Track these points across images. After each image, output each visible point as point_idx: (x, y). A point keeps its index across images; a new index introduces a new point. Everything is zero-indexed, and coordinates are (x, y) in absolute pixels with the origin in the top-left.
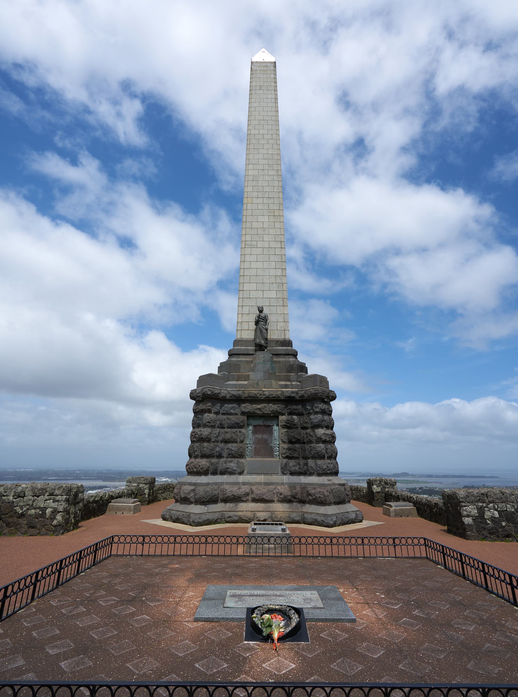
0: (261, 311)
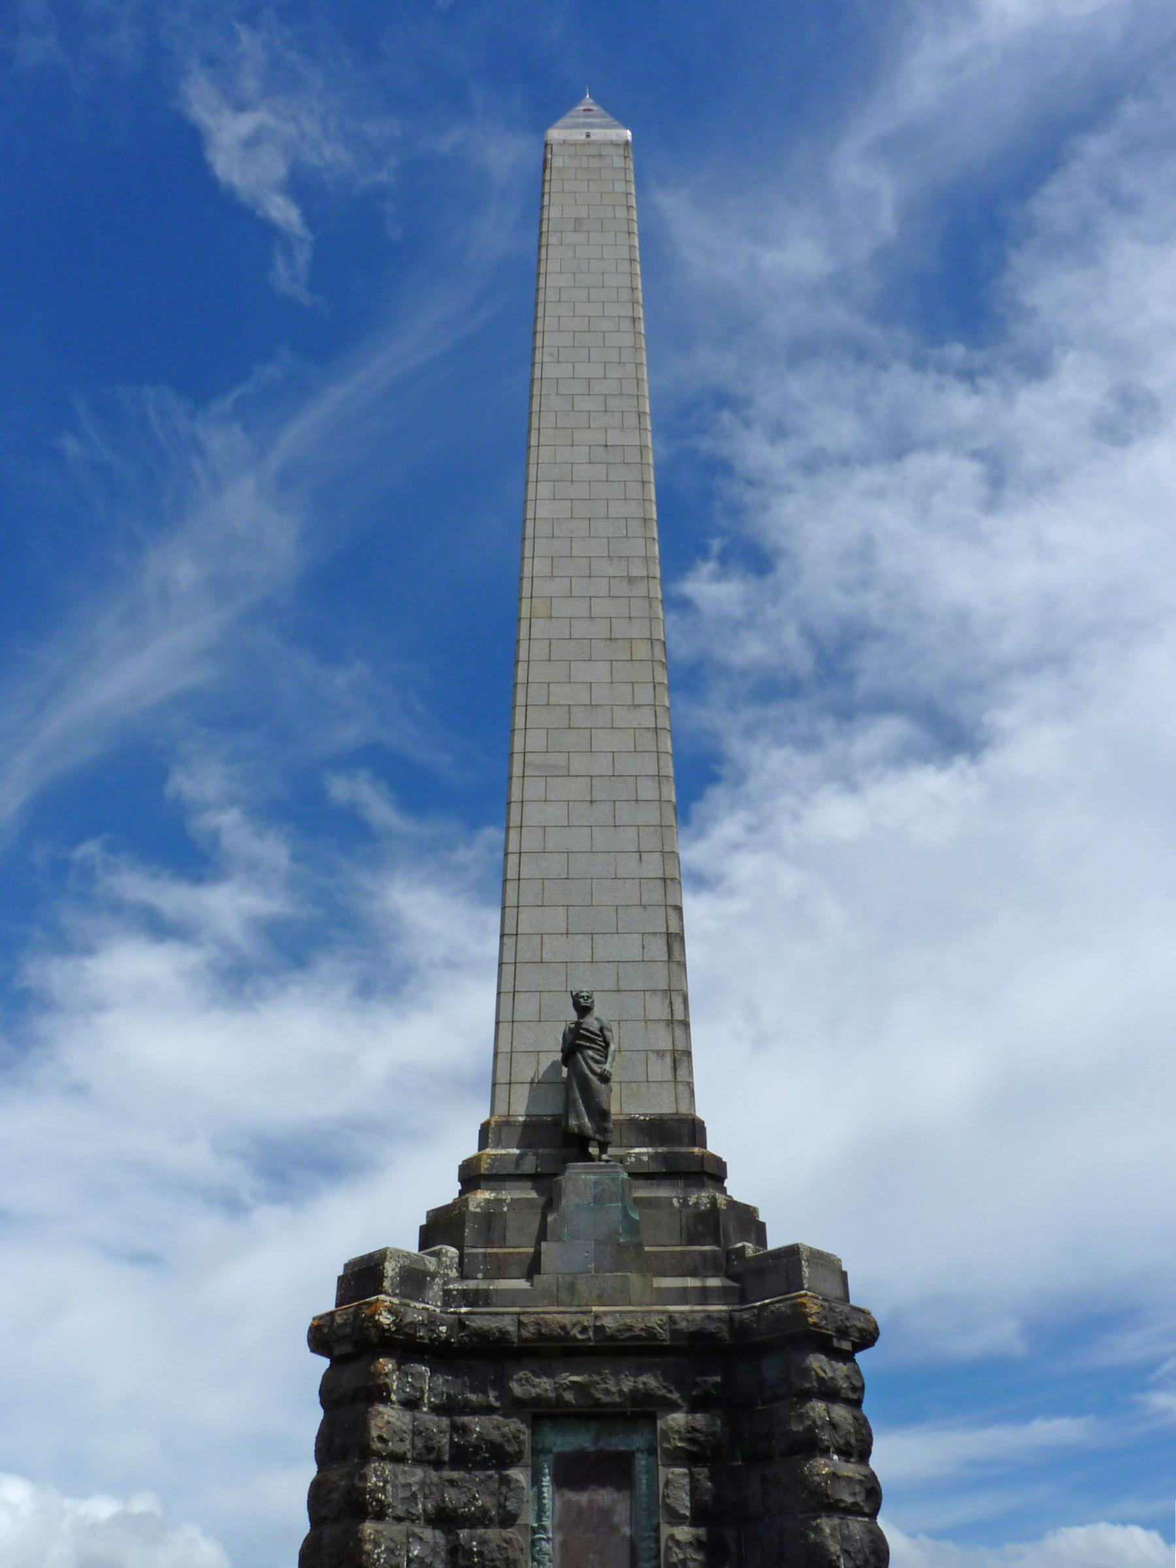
0: (583, 1009)
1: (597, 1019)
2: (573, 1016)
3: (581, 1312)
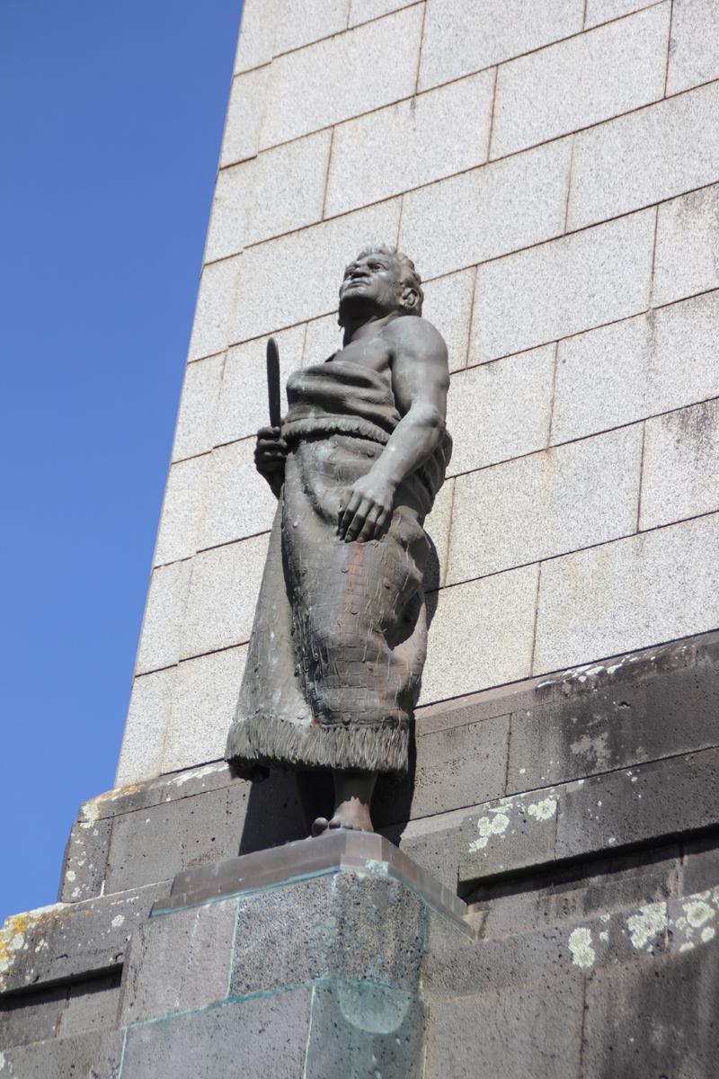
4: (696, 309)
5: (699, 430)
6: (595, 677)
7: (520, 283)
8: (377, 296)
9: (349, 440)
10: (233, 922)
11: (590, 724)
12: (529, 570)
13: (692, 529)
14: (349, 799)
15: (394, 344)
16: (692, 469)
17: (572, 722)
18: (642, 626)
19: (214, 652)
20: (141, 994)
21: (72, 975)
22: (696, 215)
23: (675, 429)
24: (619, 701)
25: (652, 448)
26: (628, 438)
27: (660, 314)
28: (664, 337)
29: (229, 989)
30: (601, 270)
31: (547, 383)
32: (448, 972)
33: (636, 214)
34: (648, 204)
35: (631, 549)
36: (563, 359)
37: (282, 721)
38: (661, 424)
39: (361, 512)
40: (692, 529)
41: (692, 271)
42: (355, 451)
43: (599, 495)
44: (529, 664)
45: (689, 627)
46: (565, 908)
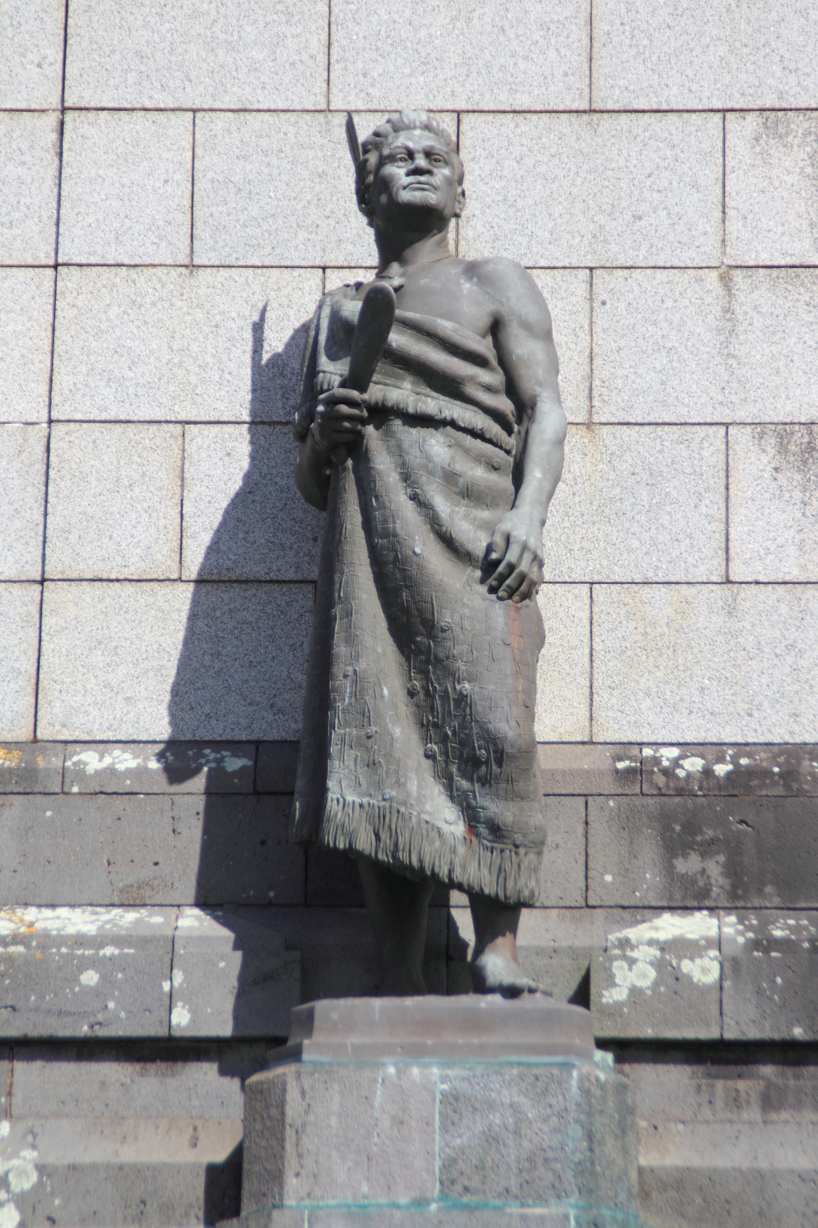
0: (403, 225)
1: (472, 269)
2: (359, 242)
3: (730, 796)
4: (790, 288)
5: (805, 462)
6: (699, 775)
7: (529, 162)
8: (444, 208)
9: (468, 440)
10: (434, 1100)
11: (699, 838)
12: (576, 591)
13: (804, 597)
14: (504, 935)
15: (501, 303)
16: (798, 515)
17: (674, 829)
18: (742, 713)
19: (101, 580)
20: (309, 1162)
21: (26, 1036)
22: (781, 149)
23: (771, 451)
24: (737, 818)
25: (740, 468)
26: (706, 444)
27: (738, 275)
28: (746, 313)
29: (438, 1185)
30: (648, 183)
31: (582, 327)
32: (672, 1194)
33: (694, 116)
34: (711, 107)
35: (720, 603)
36: (601, 298)
37: (427, 822)
38: (750, 438)
39: (511, 556)
40: (804, 597)
41: (781, 229)
42: (480, 459)
43: (669, 513)
44: (587, 724)
45: (807, 731)
46: (735, 1100)
